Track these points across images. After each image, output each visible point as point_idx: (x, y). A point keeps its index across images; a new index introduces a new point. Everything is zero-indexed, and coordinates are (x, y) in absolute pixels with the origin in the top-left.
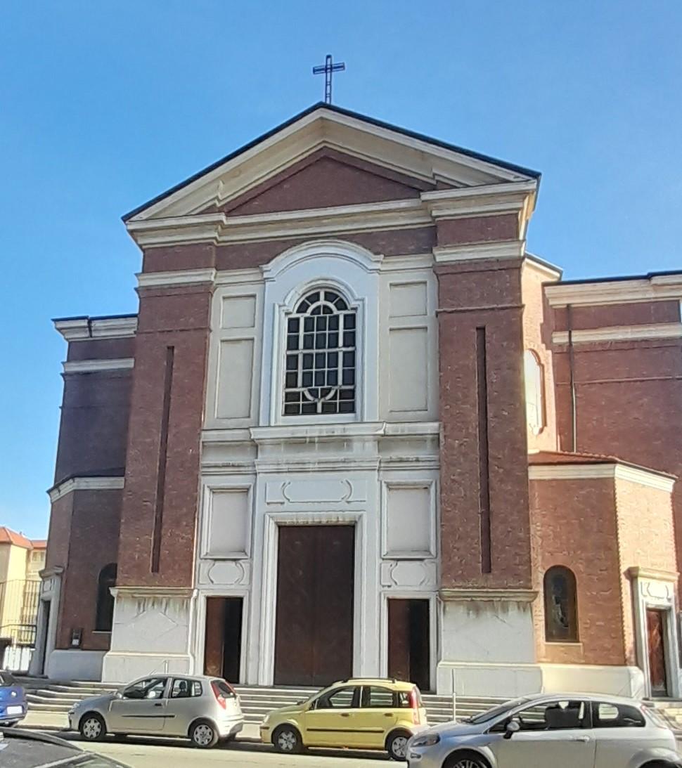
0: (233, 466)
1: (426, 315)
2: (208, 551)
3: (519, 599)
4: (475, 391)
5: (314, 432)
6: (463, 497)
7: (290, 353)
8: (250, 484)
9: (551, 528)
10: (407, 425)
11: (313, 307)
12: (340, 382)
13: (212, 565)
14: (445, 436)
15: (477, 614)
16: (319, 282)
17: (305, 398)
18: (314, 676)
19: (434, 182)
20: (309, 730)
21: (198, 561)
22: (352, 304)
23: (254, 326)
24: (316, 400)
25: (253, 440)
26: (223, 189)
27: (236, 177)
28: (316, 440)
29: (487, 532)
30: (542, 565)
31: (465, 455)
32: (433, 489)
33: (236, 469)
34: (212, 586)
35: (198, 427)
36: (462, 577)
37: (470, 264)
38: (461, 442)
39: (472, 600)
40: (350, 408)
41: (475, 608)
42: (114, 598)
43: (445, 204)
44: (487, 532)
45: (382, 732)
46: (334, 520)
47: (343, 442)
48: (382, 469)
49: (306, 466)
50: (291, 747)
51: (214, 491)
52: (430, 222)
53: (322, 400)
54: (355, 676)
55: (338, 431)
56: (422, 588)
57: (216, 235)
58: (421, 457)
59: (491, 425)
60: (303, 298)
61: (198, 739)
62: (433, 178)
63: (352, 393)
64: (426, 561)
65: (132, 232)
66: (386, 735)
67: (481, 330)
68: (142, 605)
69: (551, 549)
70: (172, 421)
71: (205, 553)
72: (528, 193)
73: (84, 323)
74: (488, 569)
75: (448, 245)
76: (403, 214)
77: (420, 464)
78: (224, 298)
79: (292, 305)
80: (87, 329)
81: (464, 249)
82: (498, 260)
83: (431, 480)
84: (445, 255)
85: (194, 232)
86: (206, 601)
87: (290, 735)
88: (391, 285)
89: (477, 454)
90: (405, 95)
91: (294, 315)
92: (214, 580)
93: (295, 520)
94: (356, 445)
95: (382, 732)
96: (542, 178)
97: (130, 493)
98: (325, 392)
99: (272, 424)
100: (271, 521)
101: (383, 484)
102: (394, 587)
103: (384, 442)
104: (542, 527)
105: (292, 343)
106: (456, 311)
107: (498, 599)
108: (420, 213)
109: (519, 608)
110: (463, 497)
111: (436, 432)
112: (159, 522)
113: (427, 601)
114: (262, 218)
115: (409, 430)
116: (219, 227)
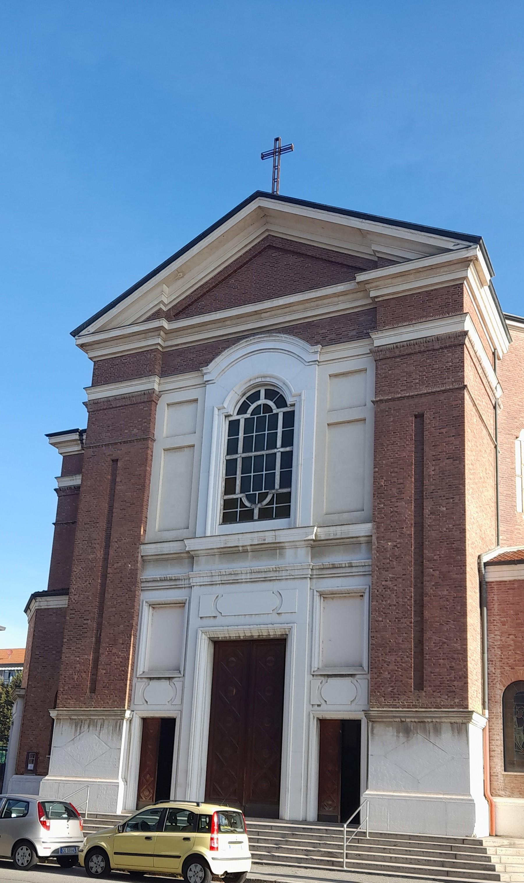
0: (171, 580)
1: (365, 405)
2: (320, 667)
3: (453, 721)
4: (410, 488)
5: (246, 541)
6: (395, 605)
7: (229, 457)
8: (186, 598)
9: (511, 637)
10: (339, 528)
11: (253, 406)
12: (277, 486)
13: (147, 684)
14: (377, 538)
15: (408, 737)
16: (257, 380)
17: (243, 505)
18: (244, 804)
19: (376, 259)
20: (116, 853)
21: (135, 680)
22: (290, 400)
23: (195, 433)
24: (253, 506)
25: (188, 552)
26: (167, 293)
27: (179, 279)
28: (249, 548)
29: (420, 642)
30: (501, 681)
31: (398, 558)
32: (366, 597)
33: (173, 583)
34: (145, 707)
35: (137, 541)
36: (394, 696)
37: (116, 399)
38: (395, 544)
39: (402, 721)
40: (285, 512)
41: (406, 730)
42: (53, 720)
43: (385, 284)
44: (420, 642)
45: (179, 857)
46: (265, 634)
47: (275, 549)
48: (315, 576)
49: (178, 583)
50: (100, 870)
51: (153, 606)
52: (369, 304)
53: (259, 506)
54: (172, 798)
55: (269, 538)
56: (353, 707)
57: (160, 341)
58: (355, 562)
59: (428, 522)
60: (244, 398)
61: (19, 860)
62: (375, 255)
63: (287, 498)
64: (358, 676)
65: (82, 346)
66: (182, 859)
67: (420, 417)
68: (79, 728)
69: (511, 661)
70: (114, 537)
71: (141, 673)
72: (471, 261)
73: (76, 436)
74: (420, 686)
75: (387, 328)
76: (341, 298)
77: (354, 570)
78: (168, 405)
79: (231, 405)
80: (79, 442)
81: (403, 330)
82: (438, 338)
83: (365, 587)
84: (384, 338)
85: (139, 340)
86: (141, 724)
87: (100, 858)
88: (330, 376)
89: (410, 558)
90: (359, 170)
91: (235, 417)
92: (148, 700)
93: (227, 636)
94: (289, 553)
95: (179, 857)
96: (485, 240)
97: (73, 612)
98: (263, 497)
99: (208, 534)
100: (204, 636)
101: (315, 593)
102: (324, 707)
103: (317, 547)
104: (501, 636)
105: (232, 447)
106: (393, 400)
107: (429, 720)
108: (360, 295)
109: (453, 729)
110: (395, 605)
111: (370, 534)
112: (98, 642)
113: (360, 721)
114: (314, 293)
115: (258, 540)
116: (162, 333)
